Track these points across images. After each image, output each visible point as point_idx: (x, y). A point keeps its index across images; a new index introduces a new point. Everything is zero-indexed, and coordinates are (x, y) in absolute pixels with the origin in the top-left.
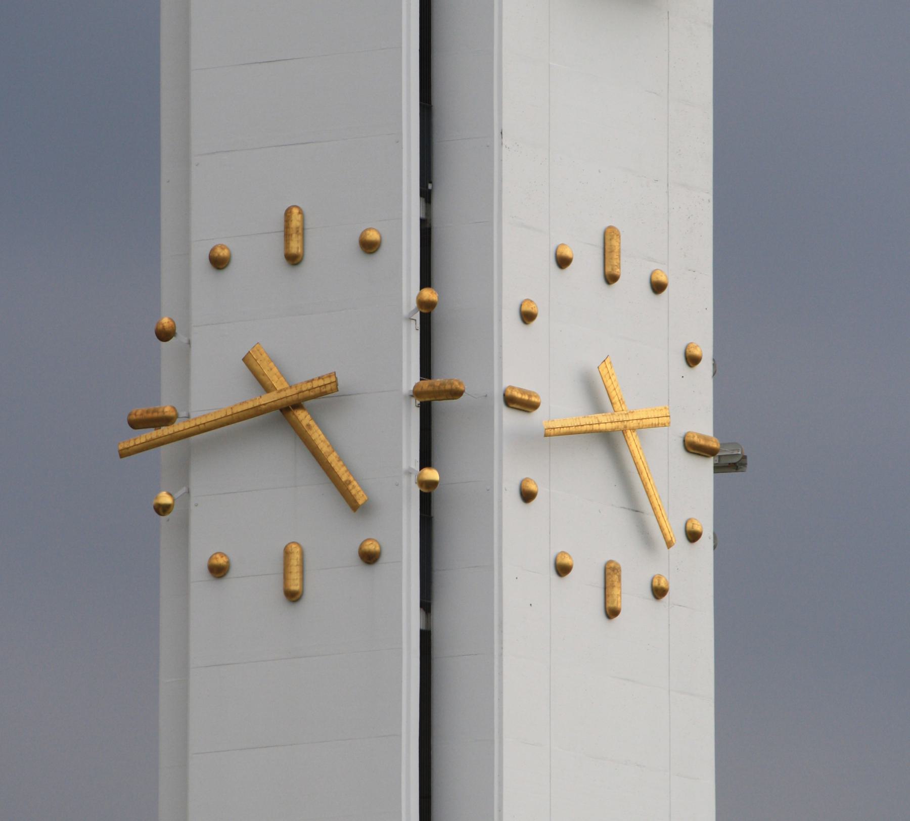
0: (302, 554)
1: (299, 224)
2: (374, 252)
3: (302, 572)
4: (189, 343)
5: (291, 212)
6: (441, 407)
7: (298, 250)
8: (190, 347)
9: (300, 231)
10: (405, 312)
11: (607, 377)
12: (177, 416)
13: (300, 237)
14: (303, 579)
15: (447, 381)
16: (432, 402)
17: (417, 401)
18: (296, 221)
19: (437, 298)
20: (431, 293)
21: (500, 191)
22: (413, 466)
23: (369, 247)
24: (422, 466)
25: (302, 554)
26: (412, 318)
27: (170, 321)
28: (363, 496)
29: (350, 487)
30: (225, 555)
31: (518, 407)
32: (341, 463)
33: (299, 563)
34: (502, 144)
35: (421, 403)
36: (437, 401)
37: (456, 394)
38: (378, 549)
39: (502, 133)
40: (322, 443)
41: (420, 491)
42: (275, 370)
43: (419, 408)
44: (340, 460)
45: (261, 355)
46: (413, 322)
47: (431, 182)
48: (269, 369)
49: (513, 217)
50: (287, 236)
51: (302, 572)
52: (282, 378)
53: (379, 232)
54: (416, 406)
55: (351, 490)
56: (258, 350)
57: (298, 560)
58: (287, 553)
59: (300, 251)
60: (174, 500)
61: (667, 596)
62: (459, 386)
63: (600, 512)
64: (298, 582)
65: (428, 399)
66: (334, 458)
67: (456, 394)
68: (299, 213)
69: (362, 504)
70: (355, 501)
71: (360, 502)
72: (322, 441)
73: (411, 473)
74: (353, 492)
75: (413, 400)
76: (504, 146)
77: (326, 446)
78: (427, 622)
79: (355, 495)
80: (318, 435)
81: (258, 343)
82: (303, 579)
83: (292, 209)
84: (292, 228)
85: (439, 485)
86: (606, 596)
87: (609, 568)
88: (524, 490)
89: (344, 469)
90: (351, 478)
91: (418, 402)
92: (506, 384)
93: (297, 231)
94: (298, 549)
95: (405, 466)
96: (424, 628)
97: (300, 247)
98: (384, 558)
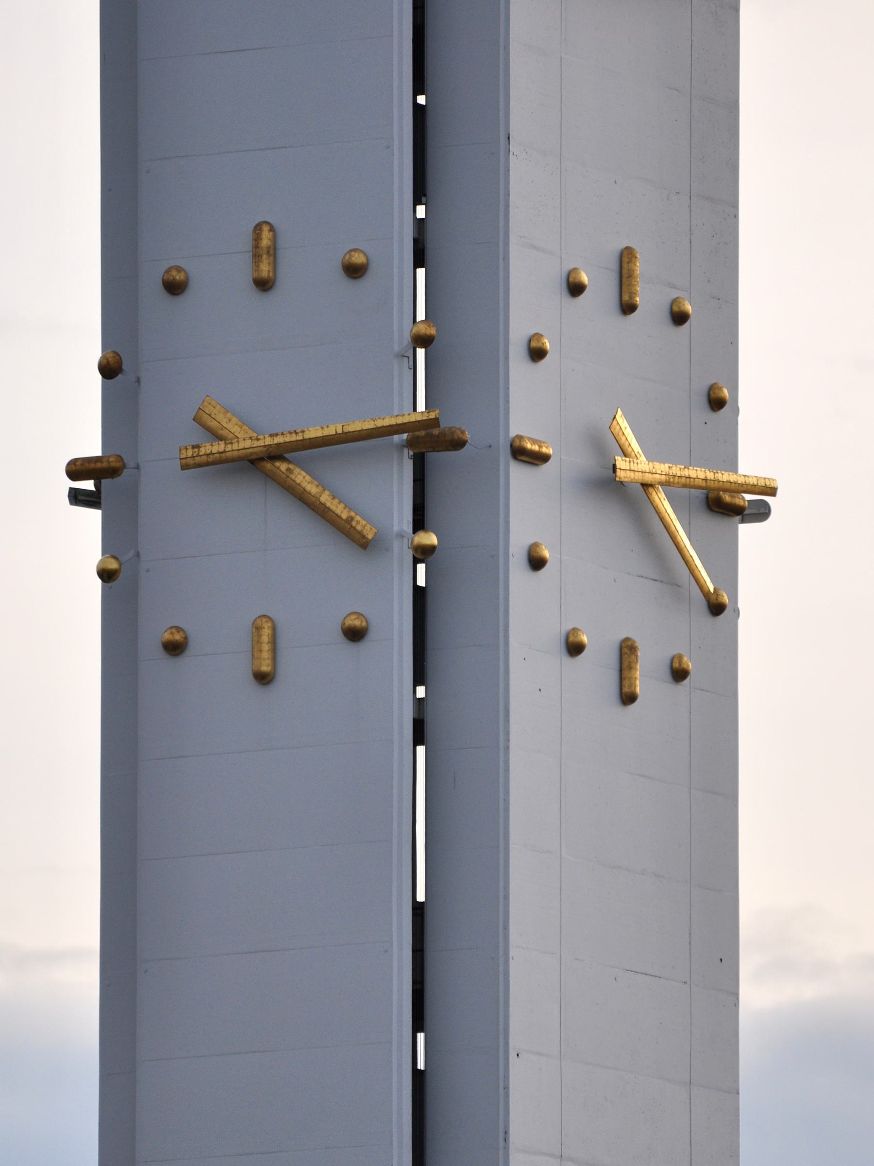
0: (274, 629)
1: (269, 243)
2: (360, 277)
3: (274, 650)
4: (138, 380)
5: (260, 229)
6: (437, 459)
7: (269, 273)
8: (139, 385)
9: (272, 252)
10: (396, 348)
11: (621, 434)
12: (124, 466)
13: (271, 259)
14: (274, 659)
15: (447, 429)
16: (426, 453)
17: (410, 451)
18: (265, 242)
19: (435, 332)
20: (428, 326)
21: (507, 206)
22: (405, 528)
23: (354, 271)
24: (415, 530)
25: (274, 629)
26: (405, 355)
27: (115, 355)
28: (371, 529)
29: (354, 523)
30: (182, 630)
31: (527, 459)
32: (336, 500)
33: (270, 640)
34: (509, 151)
35: (415, 455)
36: (435, 453)
37: (458, 444)
38: (364, 624)
39: (509, 138)
40: (309, 485)
41: (413, 555)
42: (234, 420)
43: (412, 461)
44: (334, 498)
45: (214, 408)
46: (406, 359)
47: (425, 195)
48: (228, 421)
49: (521, 237)
50: (257, 257)
51: (274, 650)
52: (245, 427)
53: (365, 254)
54: (409, 458)
55: (355, 527)
56: (210, 404)
57: (270, 636)
58: (257, 629)
59: (271, 275)
60: (120, 565)
61: (688, 679)
62: (461, 435)
63: (615, 581)
64: (269, 662)
65: (424, 450)
66: (327, 497)
67: (458, 444)
68: (270, 230)
69: (372, 538)
70: (364, 537)
71: (370, 536)
72: (309, 483)
73: (403, 536)
74: (359, 528)
75: (406, 451)
76: (511, 153)
77: (315, 487)
78: (419, 709)
79: (362, 530)
80: (302, 477)
81: (208, 396)
82: (274, 659)
83: (262, 225)
84: (262, 248)
85: (436, 550)
86: (621, 679)
87: (625, 647)
88: (533, 556)
89: (342, 506)
90: (353, 514)
91: (411, 453)
92: (513, 433)
93: (268, 252)
94: (270, 624)
95: (396, 528)
96: (417, 717)
97: (271, 270)
98: (371, 635)
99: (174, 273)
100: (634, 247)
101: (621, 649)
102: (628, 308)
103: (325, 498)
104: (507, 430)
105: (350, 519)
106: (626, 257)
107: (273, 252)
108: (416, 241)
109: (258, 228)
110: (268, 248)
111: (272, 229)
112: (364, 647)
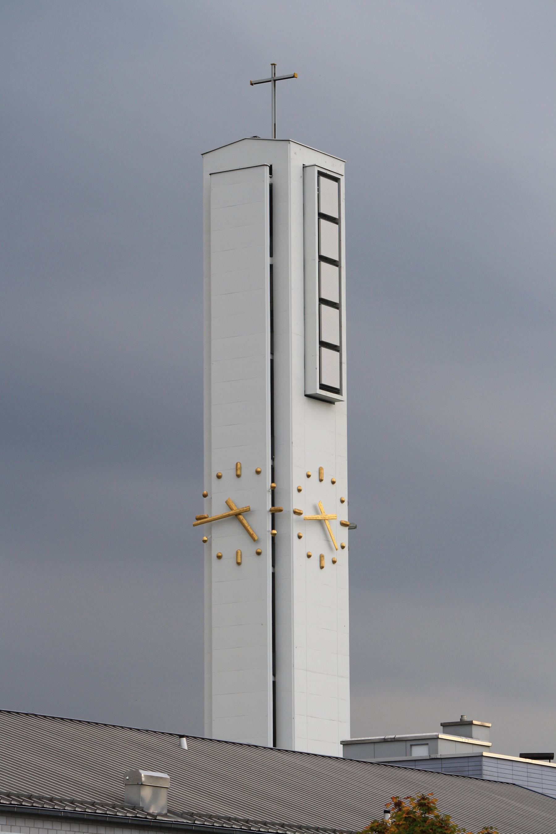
0: (241, 552)
1: (240, 467)
3: (241, 557)
4: (211, 498)
10: (267, 490)
13: (240, 470)
23: (258, 473)
24: (272, 530)
25: (241, 552)
37: (281, 511)
38: (261, 551)
42: (234, 505)
47: (274, 456)
50: (237, 470)
51: (241, 557)
53: (260, 468)
58: (237, 553)
64: (240, 560)
65: (274, 512)
67: (281, 511)
75: (270, 512)
90: (254, 533)
91: (271, 513)
92: (294, 508)
95: (268, 530)
98: (262, 554)
99: (219, 474)
100: (322, 466)
101: (320, 557)
102: (321, 480)
103: (249, 528)
104: (293, 508)
105: (253, 534)
106: (320, 469)
107: (241, 468)
108: (272, 466)
109: (237, 464)
110: (239, 468)
111: (240, 464)
112: (261, 556)
